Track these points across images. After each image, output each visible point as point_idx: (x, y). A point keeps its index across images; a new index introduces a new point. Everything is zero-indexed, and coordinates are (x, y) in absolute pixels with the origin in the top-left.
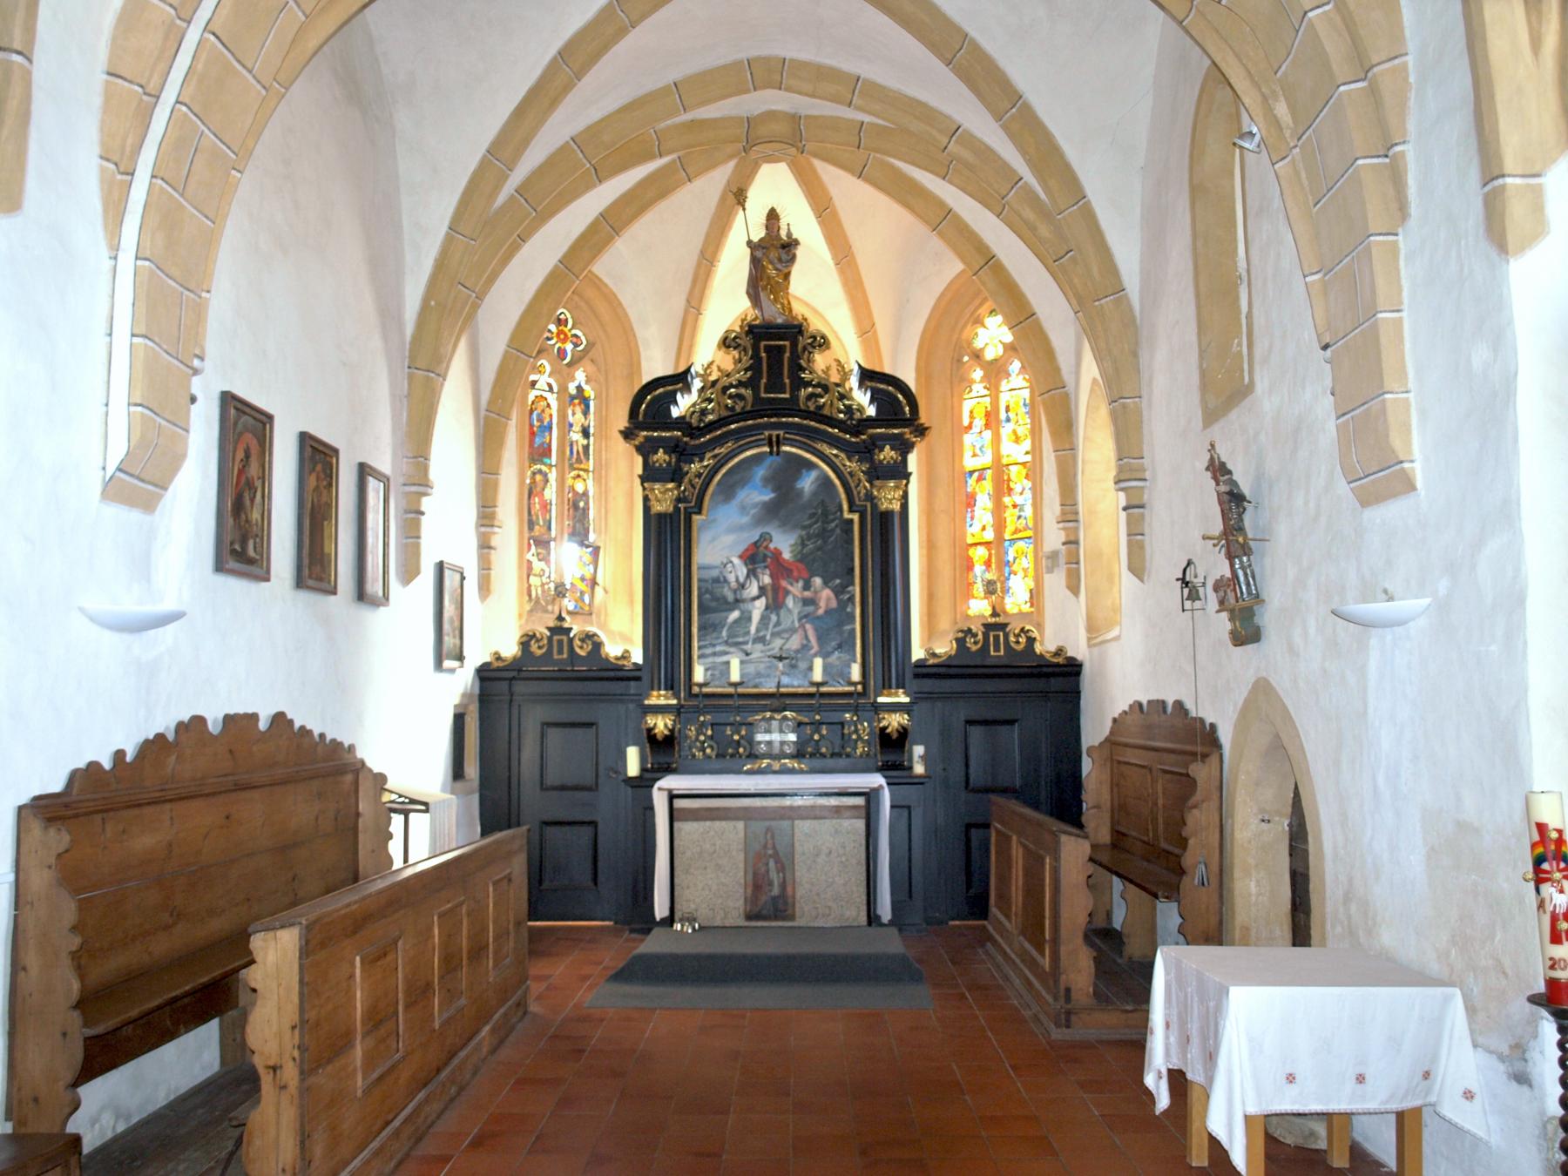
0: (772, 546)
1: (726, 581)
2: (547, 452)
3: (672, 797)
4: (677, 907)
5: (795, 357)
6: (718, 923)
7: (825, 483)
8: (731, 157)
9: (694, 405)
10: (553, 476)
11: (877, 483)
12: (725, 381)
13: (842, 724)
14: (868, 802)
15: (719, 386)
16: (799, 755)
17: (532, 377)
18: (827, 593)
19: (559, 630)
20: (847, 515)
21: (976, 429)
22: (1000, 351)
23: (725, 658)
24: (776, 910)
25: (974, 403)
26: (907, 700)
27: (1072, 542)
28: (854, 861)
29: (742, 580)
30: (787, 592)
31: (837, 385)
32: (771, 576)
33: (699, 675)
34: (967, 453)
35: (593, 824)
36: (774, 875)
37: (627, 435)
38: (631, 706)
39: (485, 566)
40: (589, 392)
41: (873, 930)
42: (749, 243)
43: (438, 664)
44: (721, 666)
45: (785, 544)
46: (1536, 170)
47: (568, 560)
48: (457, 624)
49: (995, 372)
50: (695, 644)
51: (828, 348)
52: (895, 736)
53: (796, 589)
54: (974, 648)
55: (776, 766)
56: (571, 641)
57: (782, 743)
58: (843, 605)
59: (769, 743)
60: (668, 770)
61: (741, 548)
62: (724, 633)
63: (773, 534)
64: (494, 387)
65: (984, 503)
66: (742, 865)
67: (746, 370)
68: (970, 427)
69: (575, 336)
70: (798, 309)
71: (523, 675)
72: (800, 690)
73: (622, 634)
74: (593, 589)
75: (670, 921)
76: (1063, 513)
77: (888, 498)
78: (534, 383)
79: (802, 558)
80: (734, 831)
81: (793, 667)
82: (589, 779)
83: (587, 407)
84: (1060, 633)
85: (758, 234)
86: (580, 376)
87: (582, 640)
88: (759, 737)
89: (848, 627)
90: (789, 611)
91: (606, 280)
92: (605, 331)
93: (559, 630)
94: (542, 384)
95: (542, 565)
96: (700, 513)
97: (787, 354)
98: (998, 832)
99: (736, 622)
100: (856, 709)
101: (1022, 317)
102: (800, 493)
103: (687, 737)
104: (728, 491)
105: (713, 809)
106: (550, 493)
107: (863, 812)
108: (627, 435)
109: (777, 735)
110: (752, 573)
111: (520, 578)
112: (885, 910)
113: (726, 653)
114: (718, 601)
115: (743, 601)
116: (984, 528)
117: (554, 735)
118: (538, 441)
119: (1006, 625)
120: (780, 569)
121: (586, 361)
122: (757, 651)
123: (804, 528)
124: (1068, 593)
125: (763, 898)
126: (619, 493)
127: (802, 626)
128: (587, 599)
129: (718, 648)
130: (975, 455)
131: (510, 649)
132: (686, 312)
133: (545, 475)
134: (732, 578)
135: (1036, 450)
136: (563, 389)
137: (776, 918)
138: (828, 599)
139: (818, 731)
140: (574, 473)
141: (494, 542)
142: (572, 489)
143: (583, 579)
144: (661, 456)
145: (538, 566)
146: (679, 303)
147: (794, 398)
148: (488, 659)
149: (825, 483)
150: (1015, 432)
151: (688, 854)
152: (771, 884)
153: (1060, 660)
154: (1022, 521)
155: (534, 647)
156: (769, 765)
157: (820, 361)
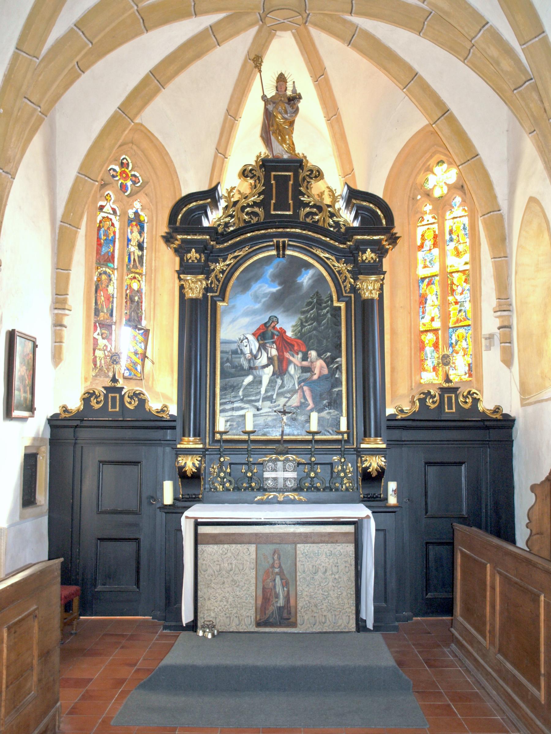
0: (278, 326)
1: (242, 352)
2: (111, 259)
3: (197, 524)
4: (200, 615)
5: (297, 185)
6: (233, 628)
7: (320, 279)
8: (251, 25)
9: (219, 219)
11: (361, 277)
12: (243, 202)
13: (331, 464)
14: (356, 529)
15: (239, 205)
16: (299, 489)
17: (101, 203)
19: (113, 390)
20: (336, 304)
21: (426, 248)
22: (445, 190)
23: (241, 413)
24: (282, 618)
25: (424, 230)
26: (384, 446)
27: (506, 327)
28: (345, 578)
29: (254, 352)
30: (289, 362)
31: (329, 206)
32: (277, 349)
33: (221, 425)
34: (420, 265)
35: (137, 540)
36: (279, 589)
37: (168, 239)
38: (168, 449)
39: (58, 340)
40: (144, 216)
41: (362, 635)
42: (264, 97)
43: (8, 414)
44: (238, 417)
45: (288, 325)
47: (125, 340)
48: (28, 382)
49: (442, 205)
50: (218, 401)
51: (322, 178)
52: (374, 474)
53: (297, 359)
54: (433, 406)
55: (281, 497)
56: (122, 397)
57: (285, 479)
58: (332, 372)
59: (275, 479)
60: (195, 499)
61: (254, 328)
62: (241, 393)
63: (279, 317)
64: (67, 204)
65: (433, 300)
66: (253, 581)
67: (260, 194)
68: (422, 246)
69: (134, 176)
70: (300, 150)
71: (85, 424)
72: (300, 438)
73: (162, 394)
74: (143, 361)
75: (193, 626)
76: (500, 305)
77: (368, 288)
78: (102, 208)
79: (301, 335)
80: (250, 551)
81: (294, 419)
82: (133, 506)
83: (142, 228)
84: (498, 393)
85: (271, 93)
86: (137, 205)
87: (131, 397)
88: (266, 475)
89: (336, 389)
90: (291, 376)
91: (156, 135)
92: (156, 173)
93: (113, 390)
94: (108, 209)
95: (105, 342)
96: (223, 300)
97: (291, 182)
98: (463, 554)
99: (249, 384)
100: (342, 453)
101: (469, 158)
102: (301, 285)
103: (210, 474)
104: (245, 285)
105: (230, 534)
106: (112, 289)
107: (352, 538)
108: (168, 239)
109: (281, 473)
110: (262, 347)
111: (87, 351)
112: (368, 613)
113: (242, 408)
114: (236, 370)
115: (255, 368)
116: (433, 319)
117: (108, 470)
118: (104, 250)
119: (457, 389)
120: (284, 344)
121: (141, 195)
122: (266, 407)
123: (303, 313)
124: (502, 365)
125: (271, 609)
126: (162, 285)
127: (301, 388)
128: (139, 368)
129: (236, 405)
130: (425, 267)
131: (75, 404)
132: (216, 157)
133: (109, 276)
134: (247, 350)
135: (475, 259)
136: (124, 213)
137: (280, 625)
138: (321, 368)
139: (312, 470)
141: (66, 321)
142: (129, 287)
143: (136, 353)
144: (193, 255)
145: (102, 342)
146: (210, 152)
147: (296, 214)
148: (58, 411)
149: (320, 279)
150: (456, 249)
151: (210, 571)
152: (277, 596)
153: (498, 416)
154: (463, 313)
155: (93, 402)
156: (275, 497)
157: (317, 187)
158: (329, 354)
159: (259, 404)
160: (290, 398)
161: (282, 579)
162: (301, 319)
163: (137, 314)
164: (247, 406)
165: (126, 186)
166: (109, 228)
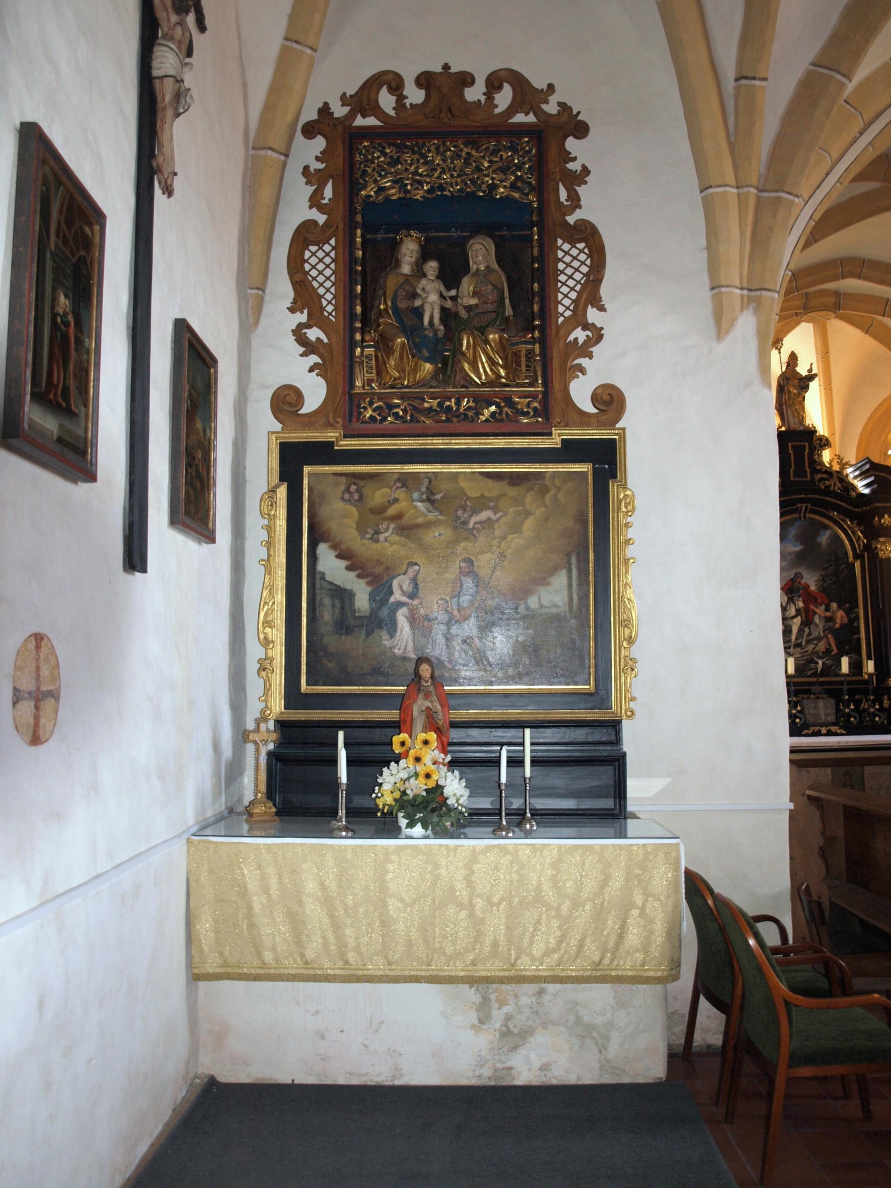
0: (803, 581)
30: (815, 613)
45: (811, 580)
53: (820, 610)
63: (804, 573)
90: (817, 625)
123: (824, 569)
127: (826, 636)
138: (842, 617)
160: (816, 645)
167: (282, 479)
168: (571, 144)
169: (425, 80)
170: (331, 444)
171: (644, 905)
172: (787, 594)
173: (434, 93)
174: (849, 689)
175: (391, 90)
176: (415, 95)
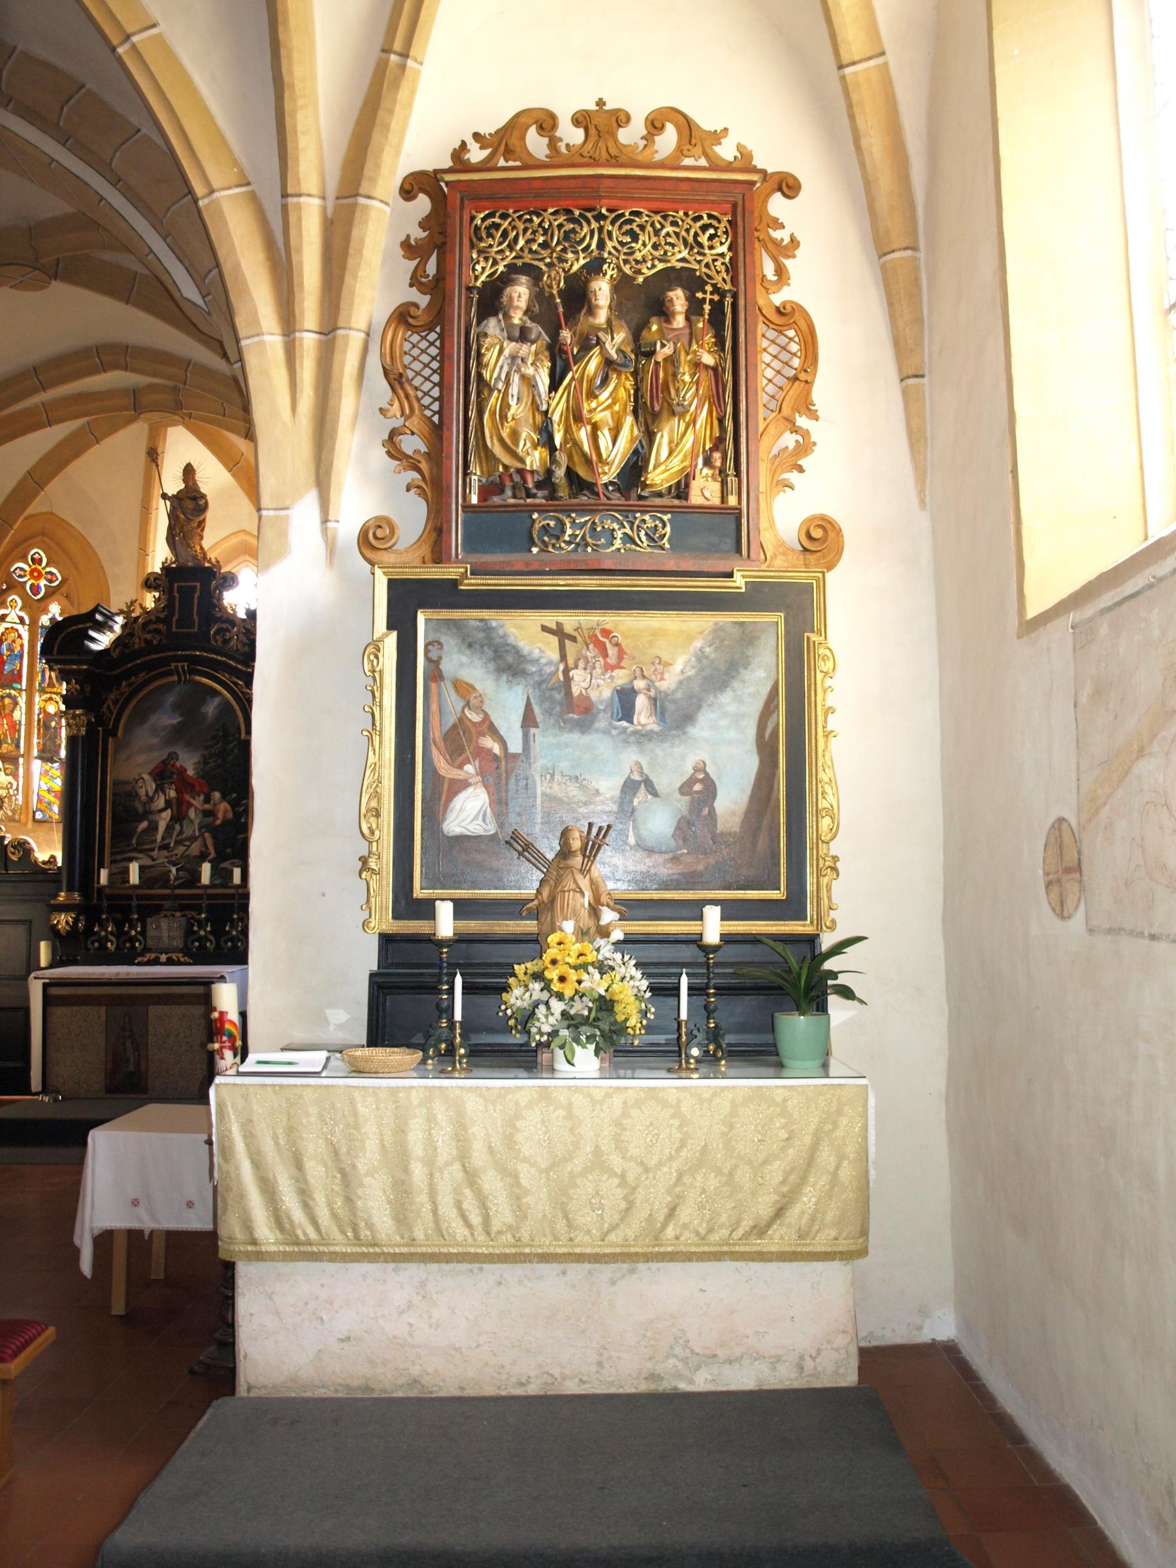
0: (178, 764)
1: (137, 795)
10: (22, 700)
18: (224, 807)
29: (151, 794)
30: (190, 805)
33: (104, 877)
45: (189, 763)
46: (287, 504)
50: (107, 850)
53: (198, 802)
61: (151, 766)
62: (134, 841)
63: (179, 753)
90: (192, 822)
99: (143, 831)
102: (204, 716)
104: (140, 717)
110: (160, 788)
115: (151, 813)
120: (185, 785)
123: (206, 748)
127: (202, 835)
134: (142, 792)
138: (226, 811)
140: (45, 696)
142: (43, 710)
158: (234, 795)
159: (155, 853)
160: (189, 847)
161: (132, 1043)
162: (203, 756)
163: (54, 742)
164: (141, 856)
165: (39, 587)
166: (14, 641)
167: (390, 627)
168: (777, 205)
169: (580, 119)
170: (455, 583)
171: (838, 1167)
172: (155, 781)
173: (593, 131)
174: (139, 905)
175: (541, 129)
176: (572, 135)
